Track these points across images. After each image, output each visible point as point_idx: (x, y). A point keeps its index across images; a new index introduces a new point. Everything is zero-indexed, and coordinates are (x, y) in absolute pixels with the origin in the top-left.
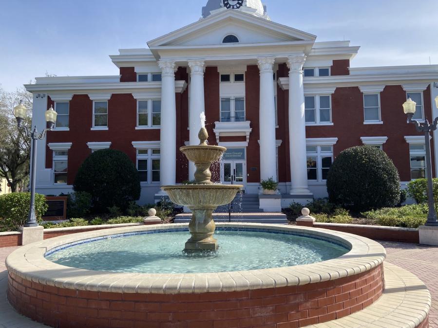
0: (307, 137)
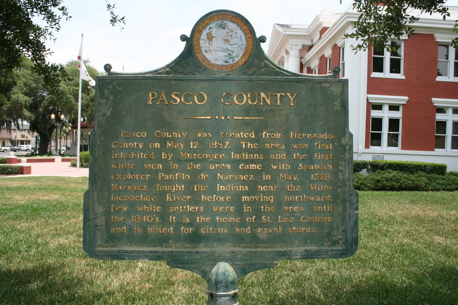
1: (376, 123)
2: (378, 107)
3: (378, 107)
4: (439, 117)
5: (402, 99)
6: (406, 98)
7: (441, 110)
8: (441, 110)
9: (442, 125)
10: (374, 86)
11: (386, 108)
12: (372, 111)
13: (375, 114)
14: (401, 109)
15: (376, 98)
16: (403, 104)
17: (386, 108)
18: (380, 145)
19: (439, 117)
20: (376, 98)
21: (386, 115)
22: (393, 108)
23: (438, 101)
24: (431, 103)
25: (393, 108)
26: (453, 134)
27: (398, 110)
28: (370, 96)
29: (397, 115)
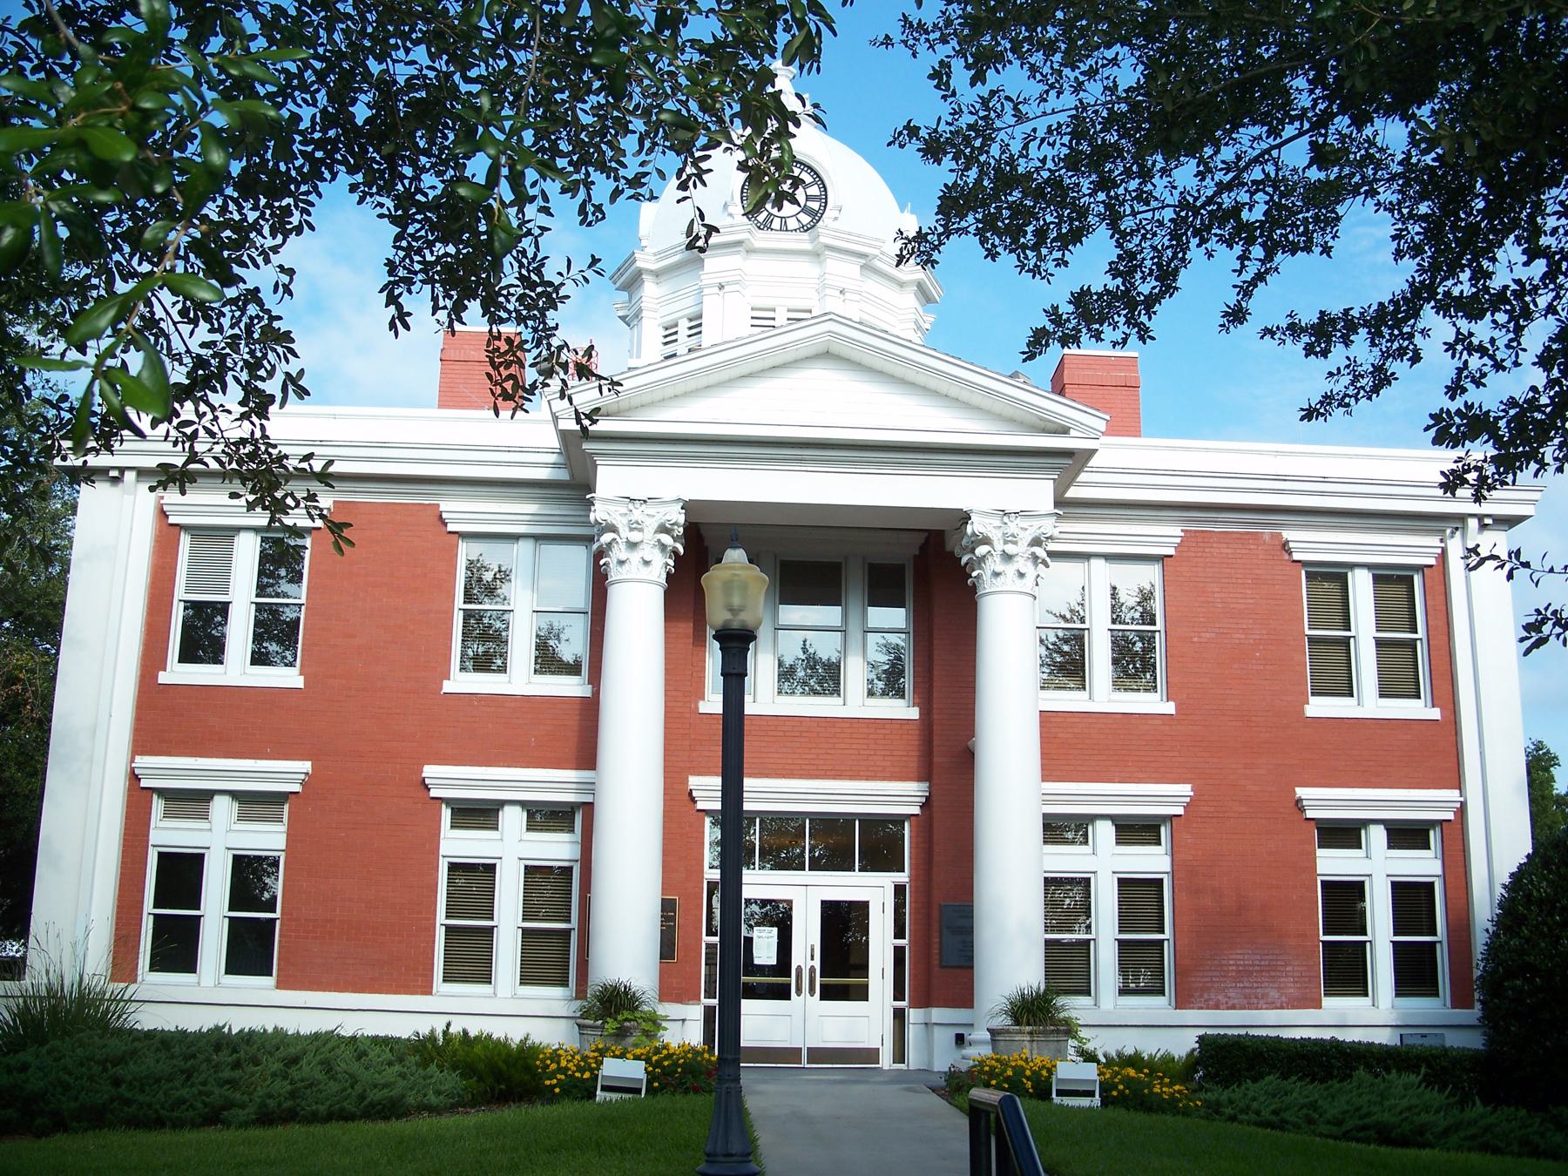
0: (1046, 777)
1: (181, 874)
2: (192, 802)
3: (192, 802)
4: (1334, 863)
5: (1166, 797)
6: (1185, 789)
7: (1344, 834)
8: (1344, 834)
9: (1345, 900)
10: (163, 720)
11: (513, 819)
12: (1320, 852)
13: (1067, 860)
14: (1434, 837)
15: (1076, 796)
16: (1441, 822)
17: (1377, 837)
18: (486, 978)
19: (1334, 863)
20: (1076, 796)
21: (220, 838)
22: (1135, 830)
23: (449, 779)
24: (1299, 805)
25: (1135, 830)
26: (1395, 934)
27: (1426, 846)
28: (142, 761)
29: (1152, 860)
